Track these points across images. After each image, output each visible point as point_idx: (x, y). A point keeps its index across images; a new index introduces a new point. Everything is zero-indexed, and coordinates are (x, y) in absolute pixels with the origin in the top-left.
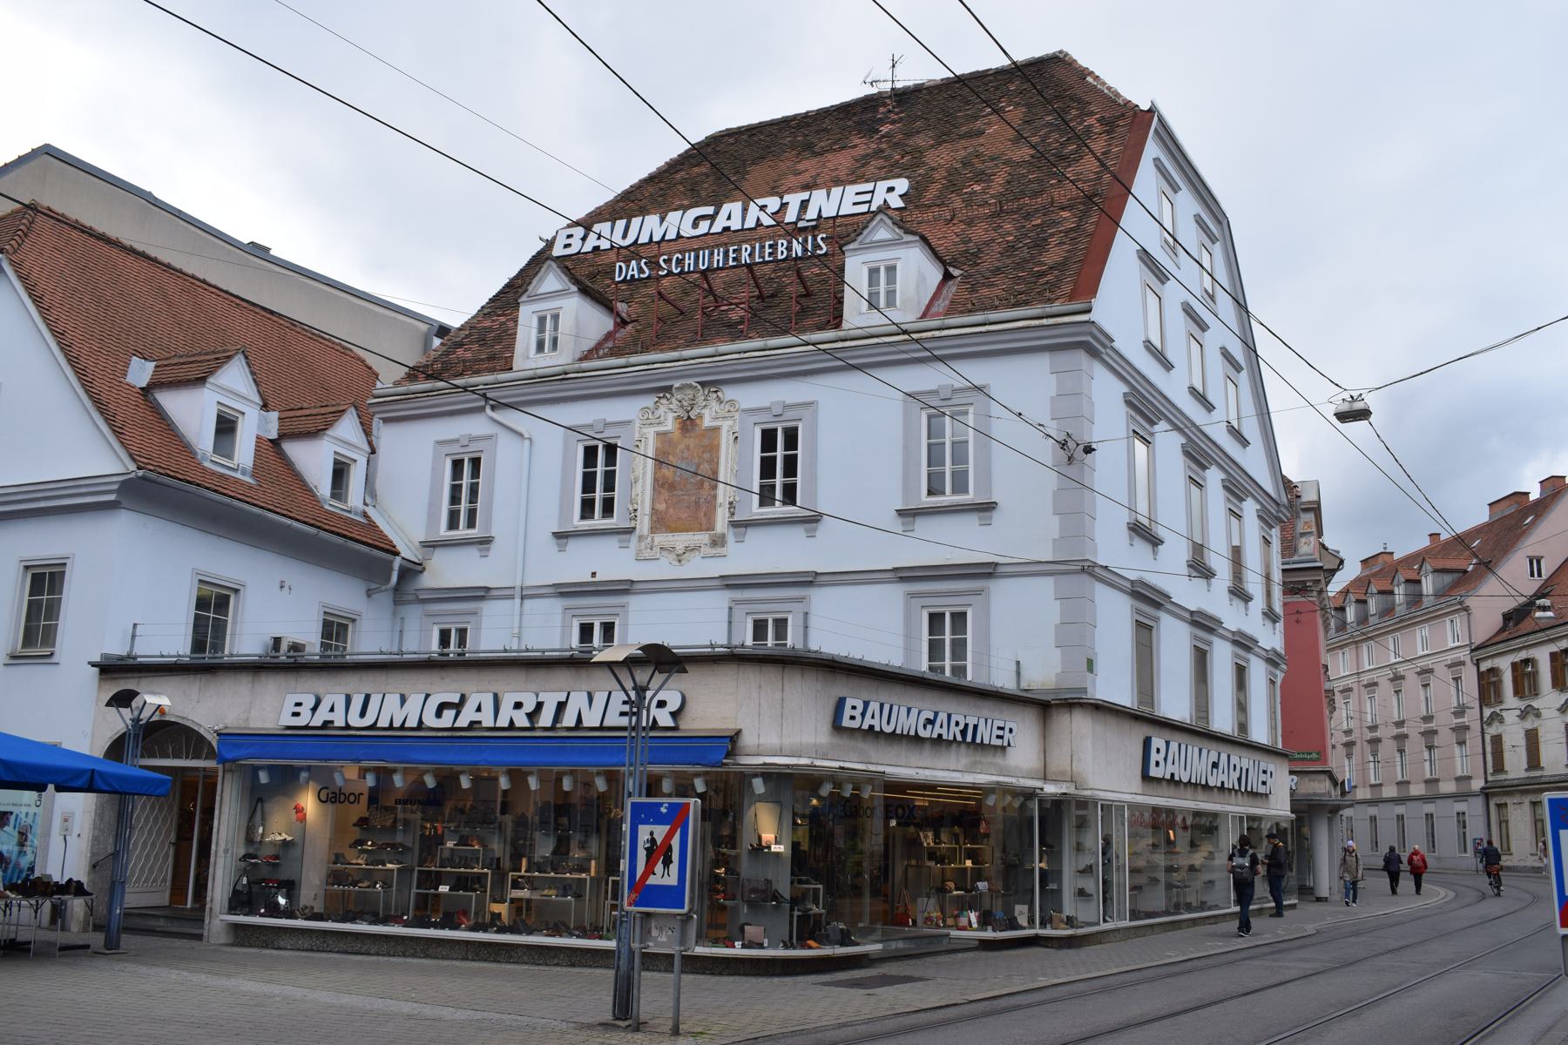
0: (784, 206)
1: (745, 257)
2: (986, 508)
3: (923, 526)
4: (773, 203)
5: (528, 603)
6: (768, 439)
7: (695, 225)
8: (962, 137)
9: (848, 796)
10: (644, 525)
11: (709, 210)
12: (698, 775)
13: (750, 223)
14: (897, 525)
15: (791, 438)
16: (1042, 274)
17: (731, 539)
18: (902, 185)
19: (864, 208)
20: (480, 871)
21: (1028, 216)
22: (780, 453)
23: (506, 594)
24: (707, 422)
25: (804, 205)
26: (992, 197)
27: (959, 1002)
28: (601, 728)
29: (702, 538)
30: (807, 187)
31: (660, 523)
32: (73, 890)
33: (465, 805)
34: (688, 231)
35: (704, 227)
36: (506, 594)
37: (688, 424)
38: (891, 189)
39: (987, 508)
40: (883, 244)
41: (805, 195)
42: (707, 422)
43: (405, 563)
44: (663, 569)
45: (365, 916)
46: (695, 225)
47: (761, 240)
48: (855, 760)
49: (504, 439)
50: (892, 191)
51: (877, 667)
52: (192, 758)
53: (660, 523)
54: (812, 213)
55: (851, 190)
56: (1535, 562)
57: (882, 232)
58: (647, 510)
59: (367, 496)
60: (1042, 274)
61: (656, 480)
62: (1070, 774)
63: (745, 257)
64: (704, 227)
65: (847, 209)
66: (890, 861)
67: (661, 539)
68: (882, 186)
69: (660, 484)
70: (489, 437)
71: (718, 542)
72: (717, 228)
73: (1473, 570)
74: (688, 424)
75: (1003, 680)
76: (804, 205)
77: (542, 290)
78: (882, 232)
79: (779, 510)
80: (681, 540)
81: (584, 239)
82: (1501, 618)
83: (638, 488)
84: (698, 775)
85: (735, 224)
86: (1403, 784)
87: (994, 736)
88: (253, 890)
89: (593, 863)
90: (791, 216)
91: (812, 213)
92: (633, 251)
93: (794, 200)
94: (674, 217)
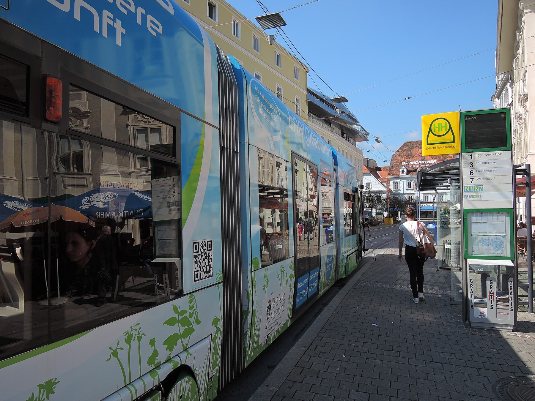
1: (421, 166)
4: (424, 161)
12: (113, 295)
13: (422, 163)
18: (436, 161)
25: (427, 162)
28: (517, 271)
30: (427, 160)
32: (137, 214)
33: (364, 253)
34: (416, 163)
35: (417, 163)
51: (78, 335)
54: (428, 163)
62: (23, 133)
63: (421, 166)
65: (431, 162)
68: (434, 161)
72: (419, 163)
73: (49, 175)
76: (427, 162)
84: (113, 295)
85: (420, 163)
89: (97, 296)
90: (426, 163)
91: (428, 163)
93: (426, 161)
94: (414, 162)
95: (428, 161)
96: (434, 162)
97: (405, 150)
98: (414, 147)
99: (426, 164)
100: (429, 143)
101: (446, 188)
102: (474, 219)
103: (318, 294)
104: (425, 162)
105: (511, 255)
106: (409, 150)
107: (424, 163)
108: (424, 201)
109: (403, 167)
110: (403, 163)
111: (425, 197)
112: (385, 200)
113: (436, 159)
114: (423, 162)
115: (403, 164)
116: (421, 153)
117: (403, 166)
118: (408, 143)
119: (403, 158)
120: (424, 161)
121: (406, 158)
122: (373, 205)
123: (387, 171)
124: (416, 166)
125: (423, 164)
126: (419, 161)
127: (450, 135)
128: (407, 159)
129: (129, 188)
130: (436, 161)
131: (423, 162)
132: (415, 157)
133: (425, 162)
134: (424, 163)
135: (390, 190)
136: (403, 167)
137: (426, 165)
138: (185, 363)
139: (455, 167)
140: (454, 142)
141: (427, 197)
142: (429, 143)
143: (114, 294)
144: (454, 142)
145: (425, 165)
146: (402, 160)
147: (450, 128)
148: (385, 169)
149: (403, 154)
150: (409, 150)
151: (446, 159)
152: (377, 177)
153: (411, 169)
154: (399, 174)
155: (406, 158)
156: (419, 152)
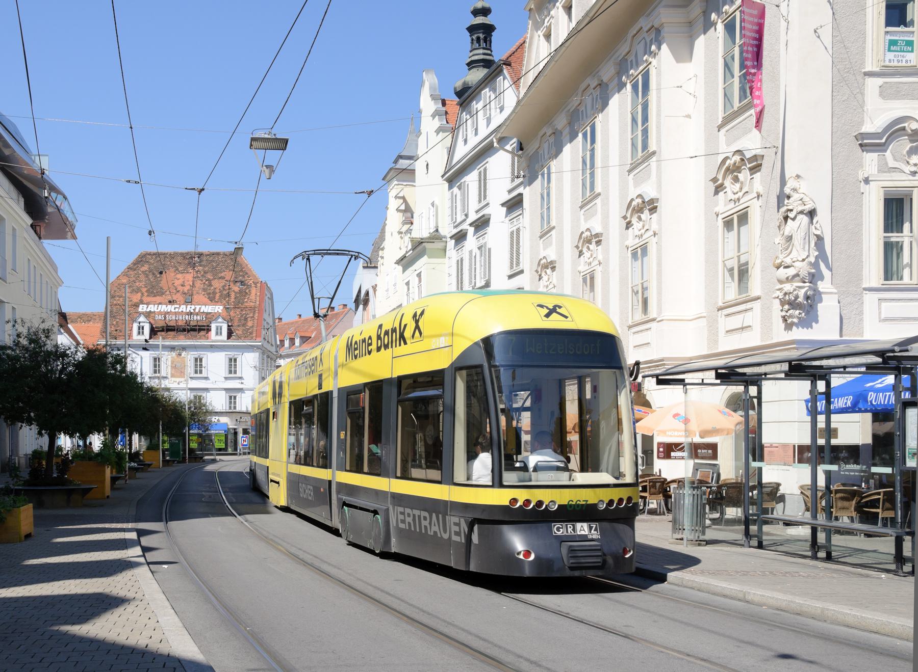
0: (196, 308)
4: (193, 307)
7: (175, 309)
8: (220, 278)
9: (197, 445)
10: (169, 376)
11: (178, 306)
13: (188, 311)
16: (249, 329)
21: (242, 310)
22: (141, 331)
25: (200, 308)
34: (173, 310)
35: (177, 310)
41: (200, 306)
45: (88, 444)
48: (157, 439)
50: (219, 309)
52: (904, 487)
53: (173, 376)
54: (202, 311)
56: (218, 420)
57: (220, 320)
59: (362, 424)
65: (210, 311)
66: (630, 408)
67: (173, 379)
68: (217, 307)
72: (180, 311)
75: (244, 410)
76: (200, 308)
78: (220, 320)
80: (178, 380)
82: (634, 362)
85: (184, 311)
90: (197, 311)
92: (160, 313)
93: (198, 307)
95: (203, 307)
97: (143, 272)
99: (197, 314)
102: (490, 484)
103: (83, 619)
104: (194, 310)
105: (49, 447)
106: (153, 274)
108: (228, 408)
109: (142, 319)
110: (141, 306)
111: (231, 397)
115: (140, 310)
116: (182, 286)
117: (140, 314)
118: (150, 254)
119: (139, 294)
125: (190, 314)
126: (182, 306)
128: (148, 296)
130: (221, 307)
131: (190, 308)
132: (168, 293)
133: (194, 310)
134: (192, 311)
135: (23, 347)
136: (142, 319)
138: (766, 447)
139: (733, 591)
141: (235, 397)
149: (137, 284)
150: (153, 274)
153: (161, 324)
154: (130, 336)
156: (177, 283)
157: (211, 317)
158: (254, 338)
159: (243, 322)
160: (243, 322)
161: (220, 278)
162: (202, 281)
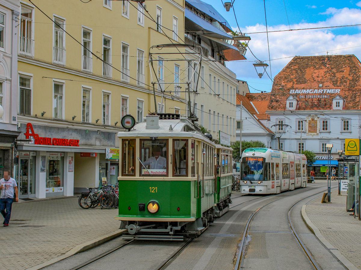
0: (324, 91)
2: (351, 132)
3: (343, 134)
4: (322, 90)
5: (292, 140)
6: (324, 122)
7: (311, 92)
8: (341, 71)
10: (307, 131)
11: (313, 90)
13: (319, 93)
14: (340, 134)
15: (326, 122)
16: (356, 103)
17: (319, 134)
18: (339, 90)
19: (334, 93)
20: (348, 169)
21: (353, 91)
22: (291, 105)
23: (289, 139)
24: (315, 119)
26: (348, 86)
27: (57, 264)
29: (315, 134)
31: (309, 131)
35: (312, 92)
36: (289, 139)
37: (313, 120)
38: (338, 91)
39: (351, 132)
40: (338, 99)
42: (315, 119)
43: (104, 93)
44: (310, 137)
46: (311, 92)
47: (321, 95)
49: (286, 119)
50: (338, 91)
53: (309, 131)
54: (327, 92)
55: (333, 90)
58: (308, 129)
60: (356, 103)
61: (309, 126)
63: (318, 97)
64: (312, 92)
68: (337, 90)
69: (309, 127)
70: (284, 119)
71: (317, 134)
74: (313, 120)
77: (290, 99)
79: (346, 131)
80: (313, 134)
81: (295, 91)
83: (306, 127)
85: (317, 92)
86: (196, 92)
87: (325, 153)
88: (103, 180)
93: (325, 90)
94: (308, 90)
96: (336, 92)
98: (307, 66)
100: (356, 150)
101: (51, 166)
107: (321, 93)
109: (291, 98)
110: (291, 90)
112: (253, 165)
113: (340, 87)
114: (321, 91)
117: (291, 95)
119: (292, 83)
120: (322, 90)
121: (296, 83)
122: (103, 197)
123: (266, 103)
124: (310, 97)
125: (320, 94)
127: (355, 148)
129: (355, 148)
130: (339, 90)
131: (321, 91)
132: (309, 81)
136: (291, 98)
137: (325, 96)
140: (357, 150)
142: (356, 150)
143: (138, 221)
144: (357, 150)
145: (323, 96)
146: (289, 85)
147: (356, 145)
148: (262, 96)
151: (353, 87)
152: (251, 111)
155: (296, 83)
156: (314, 75)
157: (332, 96)
158: (359, 108)
159: (353, 98)
160: (353, 98)
161: (341, 71)
162: (329, 73)
